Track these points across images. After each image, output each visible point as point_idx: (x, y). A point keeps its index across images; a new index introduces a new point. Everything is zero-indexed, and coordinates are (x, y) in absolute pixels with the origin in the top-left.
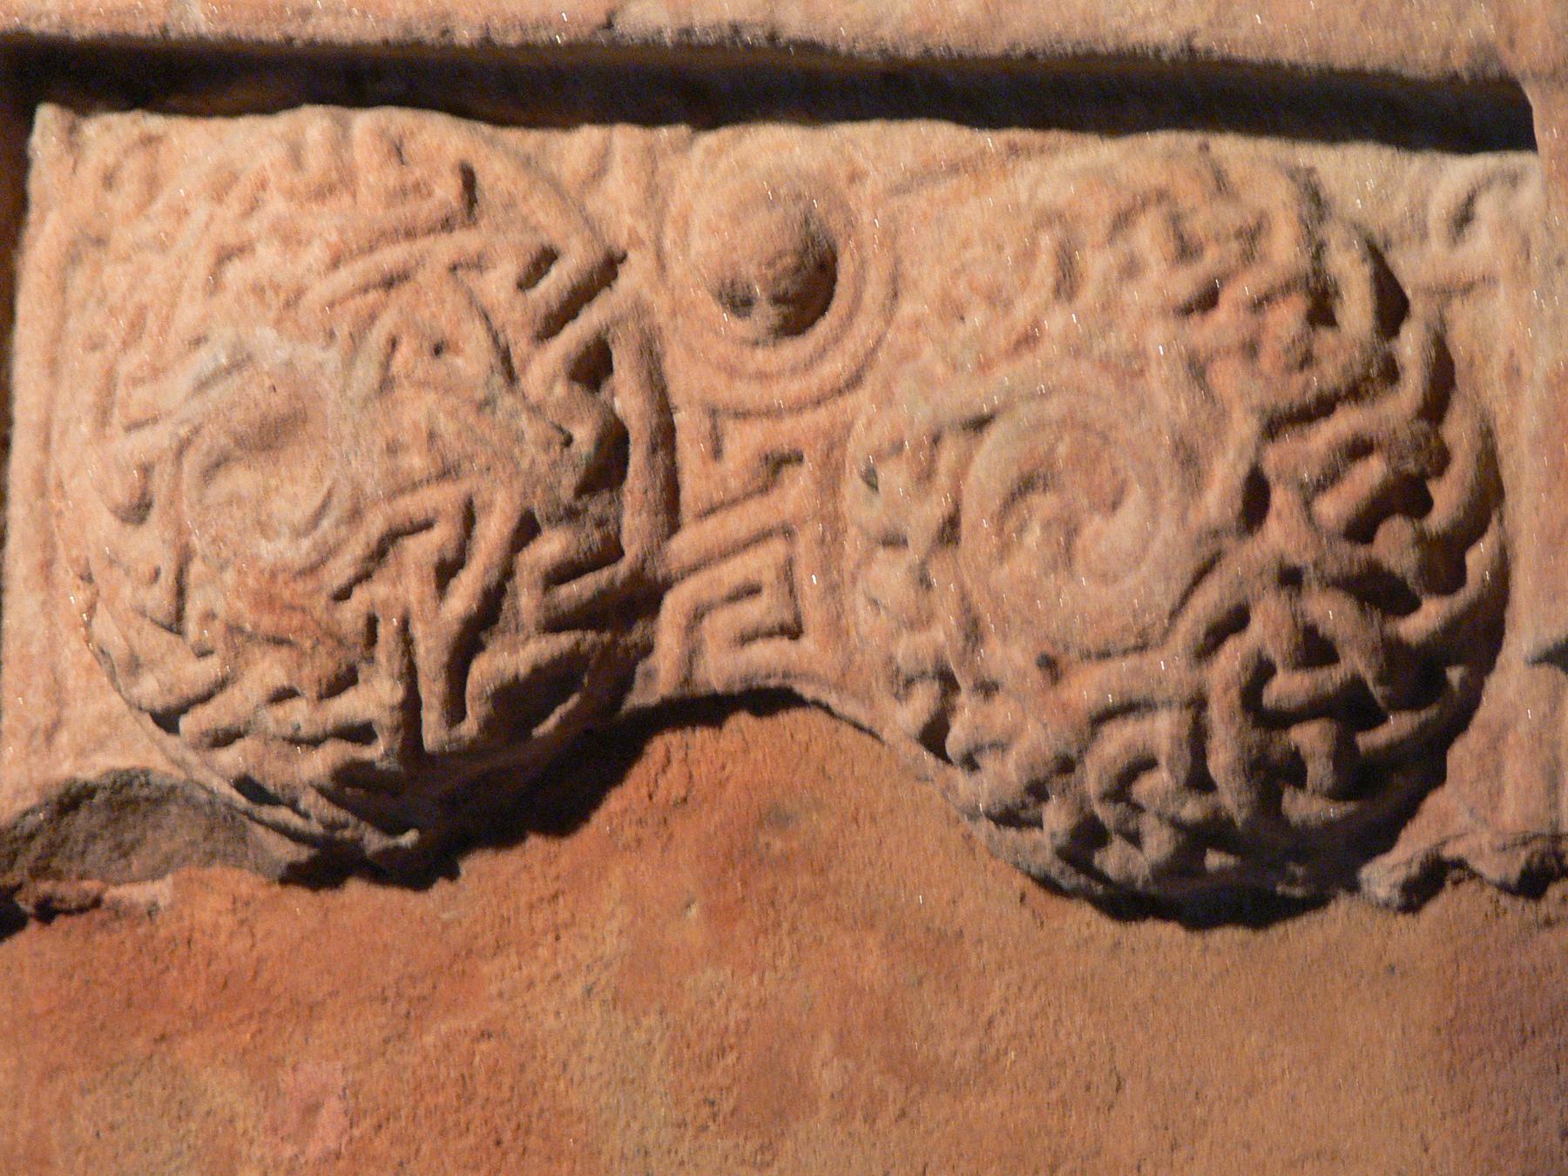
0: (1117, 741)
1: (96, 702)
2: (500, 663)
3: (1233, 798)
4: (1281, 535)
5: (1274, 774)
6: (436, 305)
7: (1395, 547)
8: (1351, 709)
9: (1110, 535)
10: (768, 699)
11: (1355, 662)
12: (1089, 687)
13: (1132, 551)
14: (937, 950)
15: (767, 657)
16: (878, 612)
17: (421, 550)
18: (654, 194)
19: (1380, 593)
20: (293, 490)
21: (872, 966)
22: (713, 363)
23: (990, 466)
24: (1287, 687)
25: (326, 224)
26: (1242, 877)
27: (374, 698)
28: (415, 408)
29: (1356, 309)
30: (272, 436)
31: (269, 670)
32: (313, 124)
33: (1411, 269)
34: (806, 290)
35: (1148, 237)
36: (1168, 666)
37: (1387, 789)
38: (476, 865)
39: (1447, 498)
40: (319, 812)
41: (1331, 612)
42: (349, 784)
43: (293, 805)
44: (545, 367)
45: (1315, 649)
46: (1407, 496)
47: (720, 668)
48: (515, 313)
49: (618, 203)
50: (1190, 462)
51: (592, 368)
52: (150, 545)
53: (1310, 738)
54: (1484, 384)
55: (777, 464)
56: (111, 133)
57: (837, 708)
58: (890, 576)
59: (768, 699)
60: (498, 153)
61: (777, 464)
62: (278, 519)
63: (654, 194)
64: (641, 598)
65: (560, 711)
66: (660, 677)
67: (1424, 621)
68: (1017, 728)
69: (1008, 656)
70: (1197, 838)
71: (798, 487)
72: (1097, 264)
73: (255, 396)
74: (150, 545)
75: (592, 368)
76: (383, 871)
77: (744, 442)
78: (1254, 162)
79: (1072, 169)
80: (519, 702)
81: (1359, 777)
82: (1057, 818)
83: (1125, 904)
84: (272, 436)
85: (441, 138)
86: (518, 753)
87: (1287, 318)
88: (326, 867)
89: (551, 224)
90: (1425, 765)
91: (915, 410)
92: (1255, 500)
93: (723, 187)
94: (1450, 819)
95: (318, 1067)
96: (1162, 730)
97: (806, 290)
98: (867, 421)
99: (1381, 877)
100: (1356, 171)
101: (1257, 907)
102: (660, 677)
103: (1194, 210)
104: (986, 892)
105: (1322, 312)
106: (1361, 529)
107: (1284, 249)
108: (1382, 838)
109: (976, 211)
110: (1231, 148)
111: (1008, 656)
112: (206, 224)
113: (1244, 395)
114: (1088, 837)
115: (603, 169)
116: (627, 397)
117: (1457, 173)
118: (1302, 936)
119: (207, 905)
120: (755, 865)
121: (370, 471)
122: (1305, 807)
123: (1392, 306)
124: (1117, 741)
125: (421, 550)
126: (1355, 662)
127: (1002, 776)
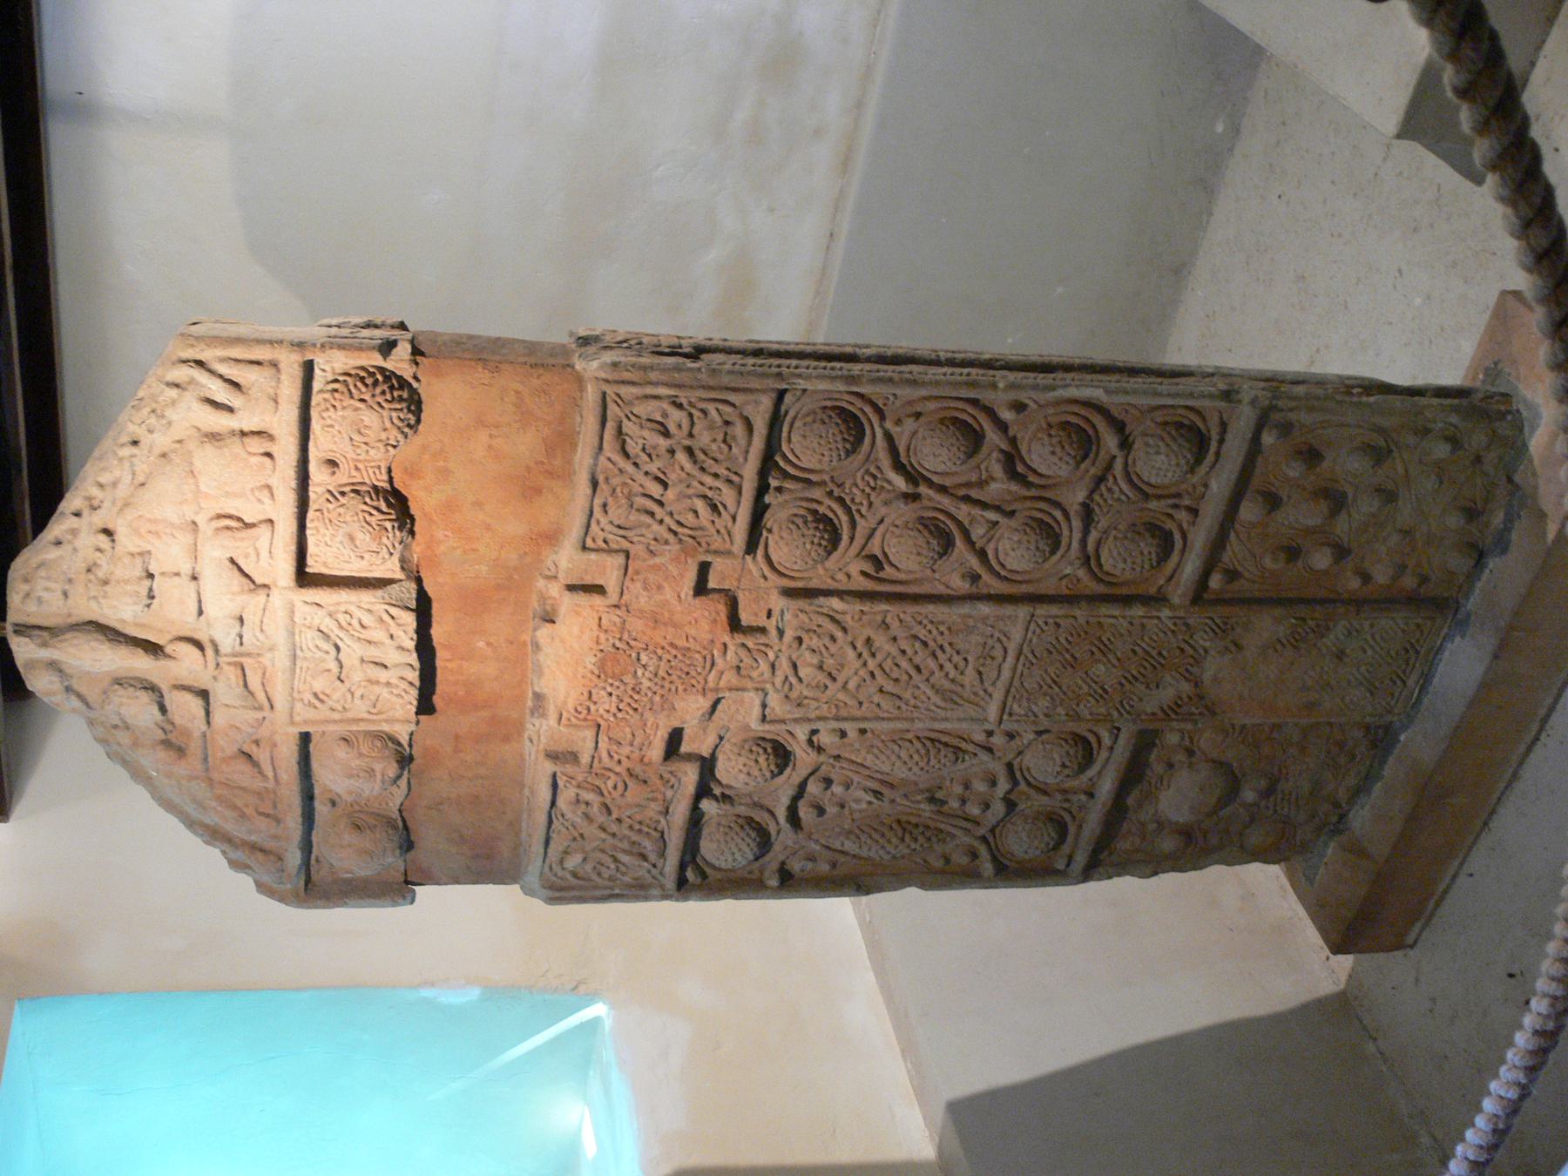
0: (396, 421)
1: (389, 565)
2: (384, 507)
3: (404, 405)
4: (367, 397)
5: (401, 399)
6: (333, 515)
7: (369, 381)
8: (392, 388)
9: (367, 421)
10: (389, 471)
11: (385, 387)
12: (388, 424)
13: (370, 418)
14: (425, 448)
15: (384, 471)
16: (377, 455)
17: (368, 518)
18: (319, 485)
19: (376, 383)
20: (360, 536)
21: (427, 457)
22: (342, 477)
23: (356, 437)
24: (388, 397)
25: (322, 530)
26: (415, 404)
27: (388, 525)
28: (348, 518)
29: (336, 386)
30: (352, 538)
31: (385, 540)
32: (308, 532)
33: (331, 378)
34: (332, 463)
35: (325, 415)
36: (385, 413)
37: (403, 383)
38: (412, 512)
39: (363, 374)
40: (404, 534)
41: (378, 390)
42: (400, 529)
43: (1204, 420)
44: (343, 500)
45: (383, 393)
46: (362, 379)
47: (385, 477)
48: (335, 504)
49: (320, 490)
50: (357, 409)
51: (343, 494)
52: (367, 556)
53: (396, 394)
54: (347, 368)
55: (357, 468)
56: (310, 561)
57: (827, 620)
58: (372, 452)
59: (389, 471)
60: (313, 506)
61: (357, 468)
62: (364, 538)
63: (319, 485)
64: (375, 488)
65: (24, 453)
66: (386, 486)
67: (379, 377)
68: (394, 435)
69: (384, 436)
70: (409, 410)
71: (360, 466)
72: (329, 422)
73: (346, 541)
74: (367, 556)
75: (343, 494)
76: (413, 524)
77: (354, 473)
78: (316, 399)
79: (316, 425)
80: (389, 505)
81: (401, 388)
82: (406, 430)
83: (418, 421)
84: (352, 538)
85: (311, 514)
86: (397, 505)
87: (337, 395)
88: (412, 533)
89: (323, 499)
90: (399, 378)
91: (349, 448)
92: (362, 400)
93: (317, 474)
94: (408, 376)
95: (440, 534)
96: (394, 414)
97: (332, 463)
98: (350, 455)
99: (415, 385)
100: (317, 385)
101: (419, 402)
102: (386, 486)
103: (1545, 995)
104: (417, 440)
105: (336, 390)
106: (366, 386)
107: (327, 396)
108: (410, 385)
109: (322, 439)
110: (313, 403)
111: (384, 436)
112: (323, 548)
113: (348, 402)
114: (409, 426)
115: (315, 492)
116: (347, 489)
117: (317, 371)
118: (423, 397)
119: (417, 550)
120: (413, 473)
121: (357, 525)
122: (405, 395)
123: (336, 381)
124: (396, 421)
125: (368, 518)
126: (385, 387)
127: (400, 437)
